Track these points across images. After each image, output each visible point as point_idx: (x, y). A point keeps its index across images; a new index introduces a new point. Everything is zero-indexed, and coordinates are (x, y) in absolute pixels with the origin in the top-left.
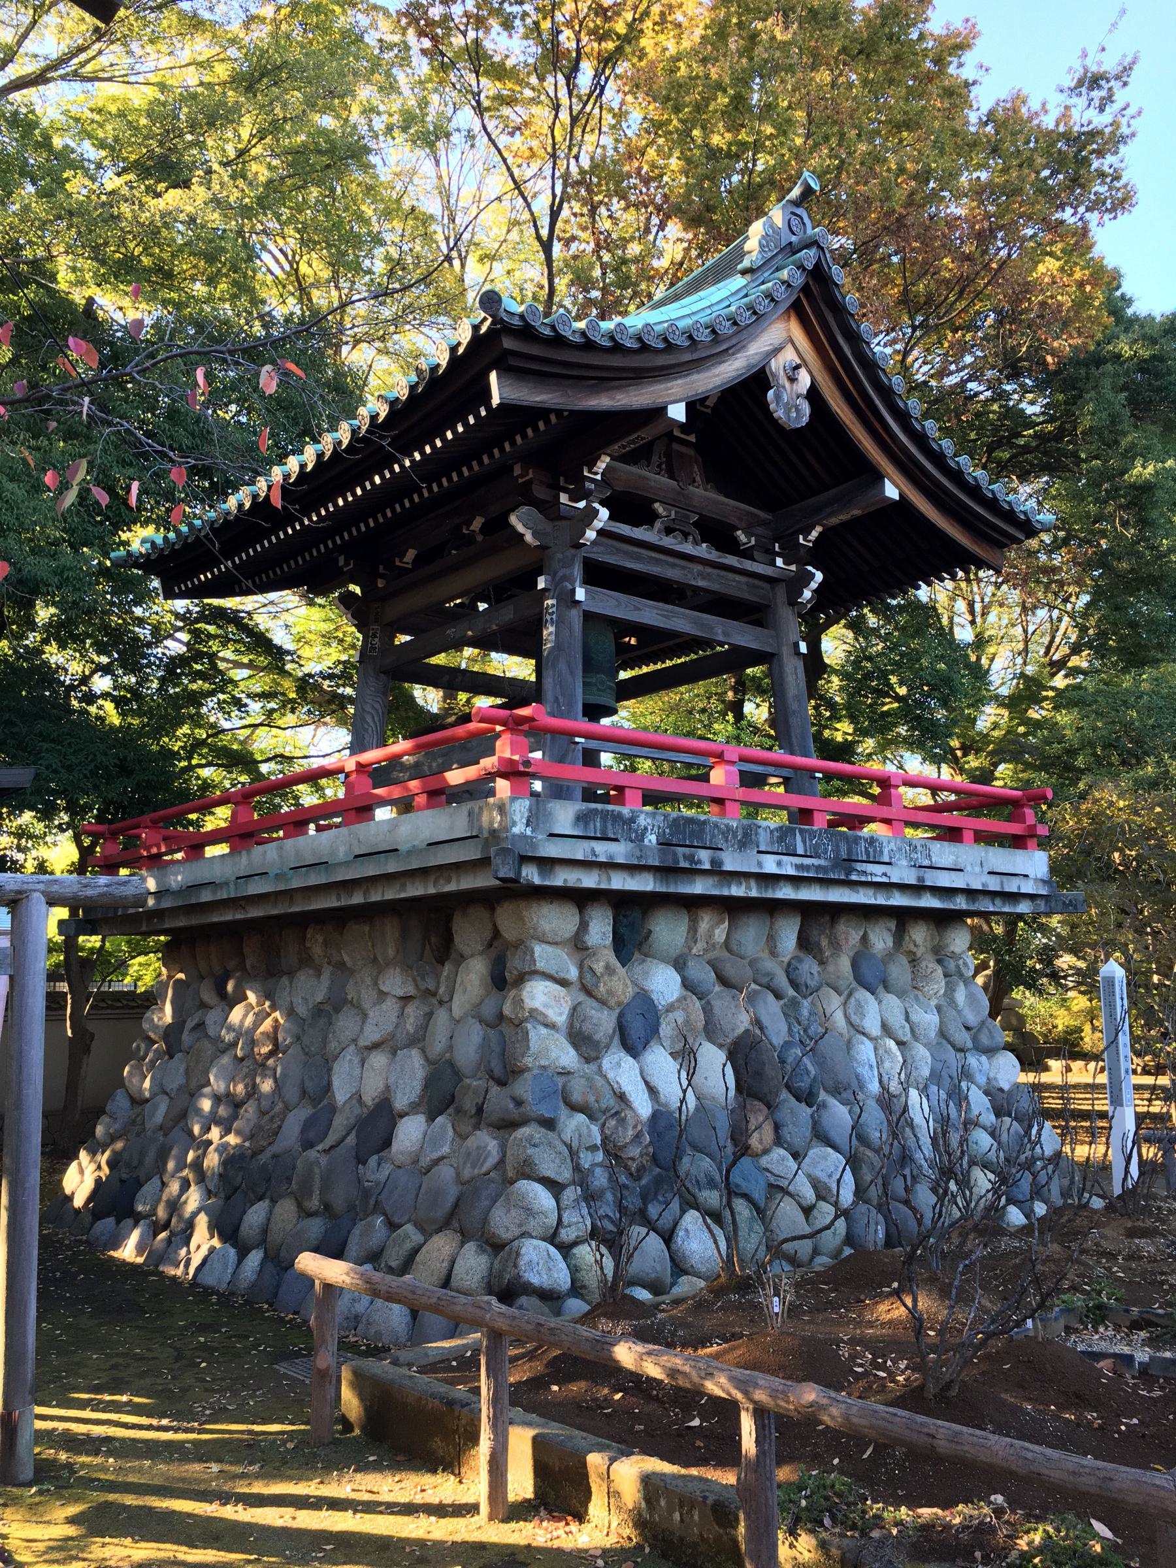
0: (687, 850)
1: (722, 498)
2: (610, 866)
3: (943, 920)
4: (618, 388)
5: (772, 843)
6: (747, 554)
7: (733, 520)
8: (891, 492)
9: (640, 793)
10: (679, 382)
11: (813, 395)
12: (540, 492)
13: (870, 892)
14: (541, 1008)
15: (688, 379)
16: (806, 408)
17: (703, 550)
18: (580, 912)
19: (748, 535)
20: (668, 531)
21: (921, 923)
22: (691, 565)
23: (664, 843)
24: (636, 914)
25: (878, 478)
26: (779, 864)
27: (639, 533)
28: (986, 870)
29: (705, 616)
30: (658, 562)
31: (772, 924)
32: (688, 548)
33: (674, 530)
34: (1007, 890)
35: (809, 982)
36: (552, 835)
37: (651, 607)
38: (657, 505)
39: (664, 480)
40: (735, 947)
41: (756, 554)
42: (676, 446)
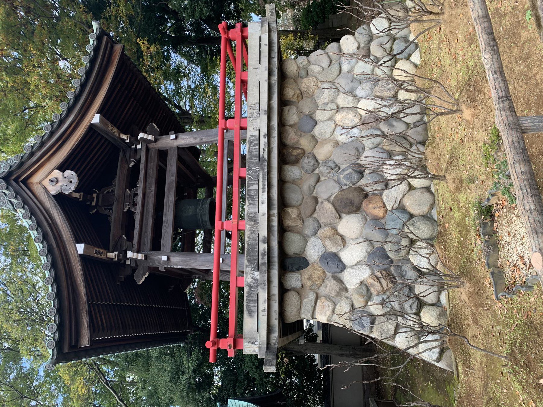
0: (260, 257)
1: (117, 177)
2: (269, 299)
3: (283, 76)
4: (76, 283)
5: (254, 204)
6: (139, 161)
7: (125, 172)
8: (96, 119)
9: (241, 169)
10: (68, 247)
11: (62, 168)
12: (128, 272)
13: (272, 139)
14: (327, 317)
15: (66, 242)
16: (68, 173)
17: (140, 185)
18: (288, 231)
19: (130, 162)
20: (135, 205)
21: (284, 92)
22: (147, 193)
23: (258, 268)
24: (288, 262)
25: (92, 127)
26: (263, 203)
27: (137, 218)
28: (259, 66)
29: (166, 186)
30: (147, 211)
31: (289, 182)
32: (140, 192)
33: (134, 202)
34: (267, 43)
35: (312, 164)
36: (258, 331)
37: (166, 214)
38: (125, 210)
39: (114, 207)
40: (298, 204)
41: (138, 157)
42: (100, 204)
